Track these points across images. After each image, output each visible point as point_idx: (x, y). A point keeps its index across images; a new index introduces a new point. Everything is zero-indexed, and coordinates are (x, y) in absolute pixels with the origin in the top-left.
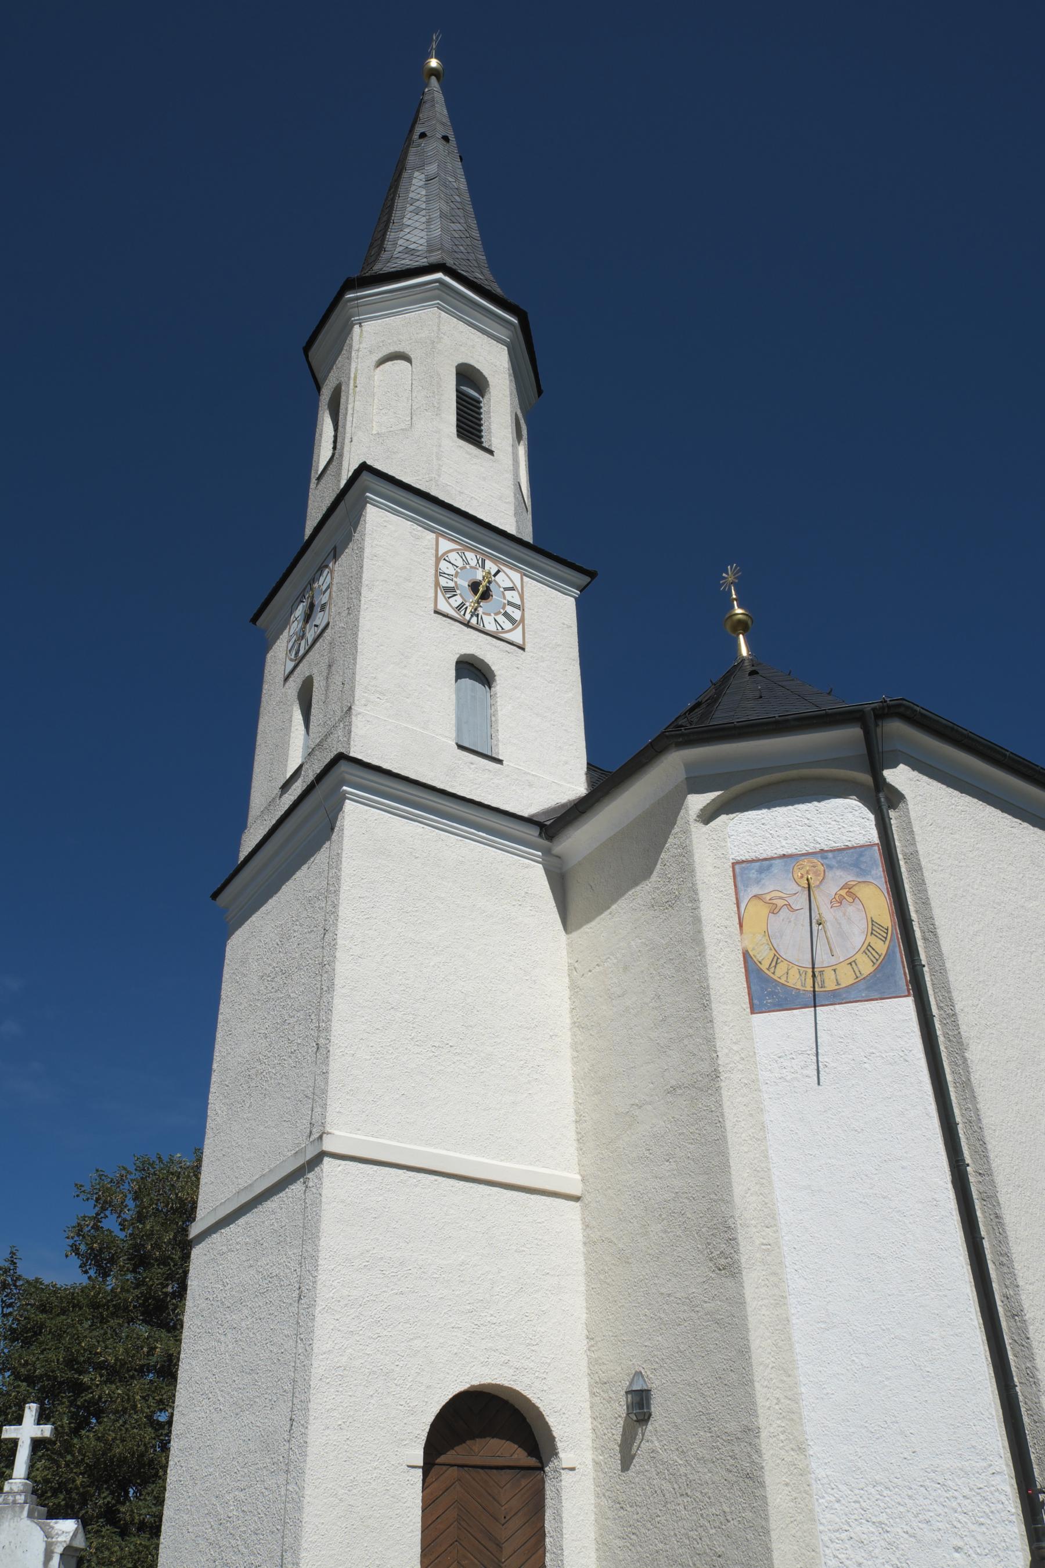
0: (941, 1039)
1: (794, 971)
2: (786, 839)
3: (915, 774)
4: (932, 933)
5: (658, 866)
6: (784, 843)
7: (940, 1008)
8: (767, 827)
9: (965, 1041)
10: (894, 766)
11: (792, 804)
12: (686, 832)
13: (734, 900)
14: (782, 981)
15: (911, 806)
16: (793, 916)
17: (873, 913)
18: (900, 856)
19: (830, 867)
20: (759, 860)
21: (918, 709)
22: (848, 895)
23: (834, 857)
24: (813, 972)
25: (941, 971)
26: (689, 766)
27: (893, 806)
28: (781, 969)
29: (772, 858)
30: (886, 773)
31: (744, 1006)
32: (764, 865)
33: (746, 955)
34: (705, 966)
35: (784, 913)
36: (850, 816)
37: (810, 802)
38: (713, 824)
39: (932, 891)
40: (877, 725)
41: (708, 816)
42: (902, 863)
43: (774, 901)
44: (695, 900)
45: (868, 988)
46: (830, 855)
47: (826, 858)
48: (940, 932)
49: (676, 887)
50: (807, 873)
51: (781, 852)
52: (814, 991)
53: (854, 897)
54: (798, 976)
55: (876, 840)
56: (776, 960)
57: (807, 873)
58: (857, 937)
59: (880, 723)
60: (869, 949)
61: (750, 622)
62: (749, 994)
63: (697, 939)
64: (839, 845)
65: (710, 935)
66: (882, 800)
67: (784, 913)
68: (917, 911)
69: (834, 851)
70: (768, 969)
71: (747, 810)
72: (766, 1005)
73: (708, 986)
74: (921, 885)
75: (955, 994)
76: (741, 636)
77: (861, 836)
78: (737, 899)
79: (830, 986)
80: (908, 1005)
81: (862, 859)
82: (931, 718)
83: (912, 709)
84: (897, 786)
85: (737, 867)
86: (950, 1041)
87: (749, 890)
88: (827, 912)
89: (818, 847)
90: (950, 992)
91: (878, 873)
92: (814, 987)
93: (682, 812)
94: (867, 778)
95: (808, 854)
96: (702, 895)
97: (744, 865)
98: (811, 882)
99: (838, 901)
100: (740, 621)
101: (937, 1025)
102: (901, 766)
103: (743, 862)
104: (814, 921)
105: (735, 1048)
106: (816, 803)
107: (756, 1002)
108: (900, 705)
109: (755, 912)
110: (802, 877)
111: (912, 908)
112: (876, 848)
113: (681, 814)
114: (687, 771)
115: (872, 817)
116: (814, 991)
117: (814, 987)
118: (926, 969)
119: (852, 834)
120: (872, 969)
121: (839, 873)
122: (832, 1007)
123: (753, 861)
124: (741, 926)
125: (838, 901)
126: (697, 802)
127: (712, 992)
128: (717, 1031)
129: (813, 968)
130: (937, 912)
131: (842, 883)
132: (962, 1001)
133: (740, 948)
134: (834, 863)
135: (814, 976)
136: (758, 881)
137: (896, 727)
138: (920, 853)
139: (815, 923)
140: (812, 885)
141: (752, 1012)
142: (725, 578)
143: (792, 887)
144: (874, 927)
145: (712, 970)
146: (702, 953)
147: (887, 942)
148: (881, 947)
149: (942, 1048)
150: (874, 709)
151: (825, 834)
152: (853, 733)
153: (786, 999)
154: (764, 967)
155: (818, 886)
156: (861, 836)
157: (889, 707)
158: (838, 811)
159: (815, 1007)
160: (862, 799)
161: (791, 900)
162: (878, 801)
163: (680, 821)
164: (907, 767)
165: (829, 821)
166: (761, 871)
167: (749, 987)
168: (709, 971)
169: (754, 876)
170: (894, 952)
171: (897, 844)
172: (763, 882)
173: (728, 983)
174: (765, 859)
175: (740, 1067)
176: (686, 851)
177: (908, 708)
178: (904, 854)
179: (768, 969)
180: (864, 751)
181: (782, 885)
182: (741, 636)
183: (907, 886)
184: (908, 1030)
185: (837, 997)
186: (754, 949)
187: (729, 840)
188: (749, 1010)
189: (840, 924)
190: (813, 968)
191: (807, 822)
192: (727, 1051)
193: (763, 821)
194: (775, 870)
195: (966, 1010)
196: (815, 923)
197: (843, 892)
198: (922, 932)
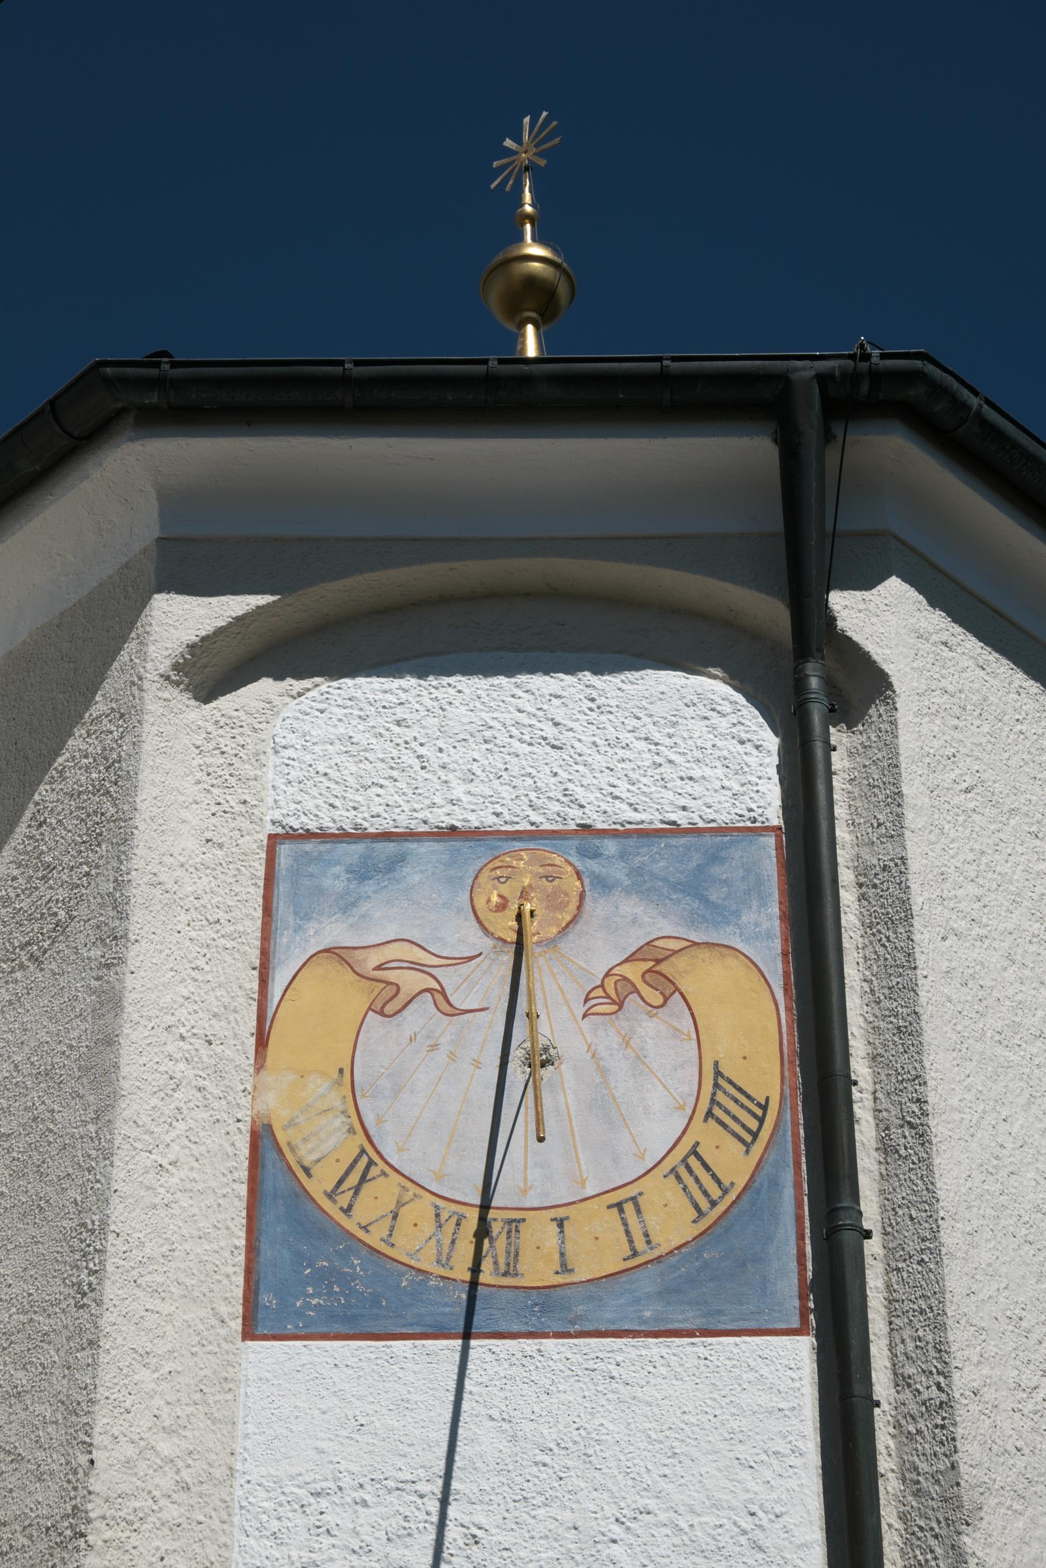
0: (890, 1488)
1: (419, 1211)
2: (470, 777)
3: (936, 621)
4: (911, 1133)
5: (22, 829)
6: (459, 791)
7: (901, 1381)
8: (409, 734)
9: (968, 1497)
10: (867, 581)
11: (510, 671)
12: (128, 716)
13: (254, 957)
14: (374, 1239)
15: (905, 714)
16: (446, 1029)
17: (723, 1047)
18: (846, 876)
19: (603, 885)
20: (359, 836)
21: (974, 401)
22: (653, 976)
23: (622, 855)
24: (483, 1219)
25: (922, 1256)
26: (174, 501)
27: (847, 710)
28: (376, 1199)
29: (411, 835)
30: (839, 601)
31: (224, 1310)
32: (379, 852)
33: (262, 1139)
34: (108, 1156)
35: (422, 1016)
36: (699, 728)
37: (571, 670)
38: (225, 703)
39: (932, 993)
40: (828, 437)
41: (214, 671)
42: (848, 897)
43: (392, 976)
44: (114, 938)
45: (667, 1293)
46: (611, 846)
47: (596, 855)
48: (938, 1127)
49: (62, 894)
50: (524, 894)
51: (441, 817)
52: (474, 1284)
53: (669, 989)
54: (428, 1227)
55: (774, 816)
56: (367, 1164)
57: (524, 894)
58: (658, 1115)
59: (838, 429)
60: (688, 1164)
61: (563, 290)
62: (249, 1271)
63: (95, 1069)
64: (649, 817)
65: (143, 1056)
66: (813, 689)
67: (422, 1016)
68: (874, 1058)
69: (627, 834)
70: (330, 1196)
71: (352, 674)
72: (299, 1314)
73: (104, 1224)
74: (898, 969)
75: (957, 1337)
76: (530, 329)
77: (725, 796)
78: (265, 954)
79: (537, 1269)
80: (798, 1355)
81: (716, 870)
82: (1015, 445)
83: (953, 397)
84: (869, 646)
85: (284, 850)
86: (918, 1493)
87: (312, 928)
88: (558, 1013)
89: (575, 816)
90: (943, 1327)
91: (762, 928)
92: (476, 1269)
93: (130, 646)
94: (771, 612)
95: (537, 835)
96: (140, 921)
97: (309, 846)
98: (531, 927)
99: (612, 996)
100: (531, 282)
101: (884, 1439)
102: (894, 584)
103: (309, 835)
104: (517, 1054)
105: (166, 1447)
106: (587, 676)
107: (266, 1298)
108: (916, 375)
109: (322, 1005)
110: (502, 906)
111: (858, 1047)
112: (771, 841)
113: (124, 656)
114: (165, 516)
115: (772, 742)
116: (474, 1284)
117: (476, 1269)
118: (873, 1247)
119: (697, 789)
120: (690, 1232)
121: (630, 906)
122: (530, 1345)
123: (343, 836)
124: (262, 1040)
125: (612, 996)
126: (181, 620)
127: (114, 1245)
128: (107, 1376)
129: (485, 1206)
130: (940, 1065)
131: (635, 941)
132: (980, 1364)
133: (245, 1114)
134: (618, 872)
135: (483, 1231)
136: (347, 905)
137: (892, 454)
138: (914, 865)
139: (522, 1060)
140: (530, 940)
141: (249, 1333)
142: (510, 152)
143: (461, 935)
144: (719, 1096)
145: (128, 1172)
146: (103, 1115)
147: (758, 1149)
148: (734, 1163)
149: (889, 1515)
150: (823, 379)
151: (605, 779)
152: (738, 455)
153: (375, 1300)
154: (317, 1187)
155: (551, 943)
156: (725, 796)
157: (876, 376)
158: (660, 709)
159: (467, 1335)
160: (740, 679)
161: (449, 978)
162: (800, 685)
163: (114, 681)
164: (912, 593)
165: (626, 737)
166: (362, 873)
167: (252, 1249)
168: (118, 1173)
169: (339, 886)
170: (774, 1184)
171: (842, 833)
172: (365, 907)
173: (175, 1214)
174: (386, 836)
175: (172, 1513)
176: (116, 777)
177: (939, 390)
178: (862, 871)
179: (330, 1196)
180: (772, 519)
181: (428, 921)
182: (530, 329)
183: (853, 974)
184: (781, 1446)
185: (556, 1313)
186: (292, 1123)
187: (272, 759)
188: (237, 1325)
189: (604, 1072)
190: (485, 1206)
191: (550, 731)
192: (130, 1451)
193: (400, 713)
194: (412, 875)
195: (989, 1394)
196: (522, 1060)
197: (634, 972)
198: (883, 1127)
